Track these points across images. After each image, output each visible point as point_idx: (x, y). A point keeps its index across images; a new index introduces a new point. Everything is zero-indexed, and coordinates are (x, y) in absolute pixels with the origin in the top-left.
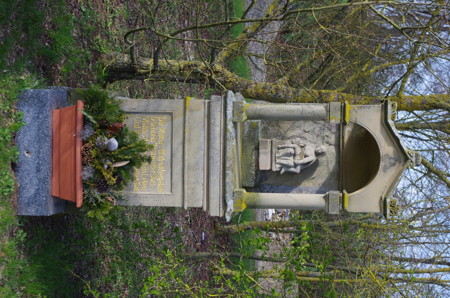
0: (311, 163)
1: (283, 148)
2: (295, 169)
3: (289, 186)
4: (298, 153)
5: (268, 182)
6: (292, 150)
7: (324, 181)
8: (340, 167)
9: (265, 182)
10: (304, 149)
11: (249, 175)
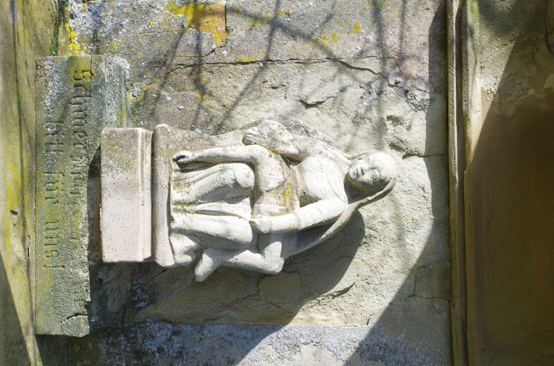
0: (331, 230)
1: (203, 163)
2: (258, 256)
3: (246, 327)
4: (273, 184)
5: (162, 309)
6: (242, 174)
7: (386, 302)
8: (449, 245)
9: (152, 310)
10: (301, 170)
11: (63, 287)
